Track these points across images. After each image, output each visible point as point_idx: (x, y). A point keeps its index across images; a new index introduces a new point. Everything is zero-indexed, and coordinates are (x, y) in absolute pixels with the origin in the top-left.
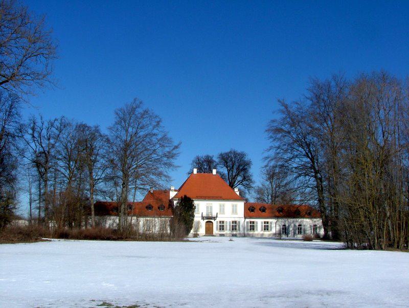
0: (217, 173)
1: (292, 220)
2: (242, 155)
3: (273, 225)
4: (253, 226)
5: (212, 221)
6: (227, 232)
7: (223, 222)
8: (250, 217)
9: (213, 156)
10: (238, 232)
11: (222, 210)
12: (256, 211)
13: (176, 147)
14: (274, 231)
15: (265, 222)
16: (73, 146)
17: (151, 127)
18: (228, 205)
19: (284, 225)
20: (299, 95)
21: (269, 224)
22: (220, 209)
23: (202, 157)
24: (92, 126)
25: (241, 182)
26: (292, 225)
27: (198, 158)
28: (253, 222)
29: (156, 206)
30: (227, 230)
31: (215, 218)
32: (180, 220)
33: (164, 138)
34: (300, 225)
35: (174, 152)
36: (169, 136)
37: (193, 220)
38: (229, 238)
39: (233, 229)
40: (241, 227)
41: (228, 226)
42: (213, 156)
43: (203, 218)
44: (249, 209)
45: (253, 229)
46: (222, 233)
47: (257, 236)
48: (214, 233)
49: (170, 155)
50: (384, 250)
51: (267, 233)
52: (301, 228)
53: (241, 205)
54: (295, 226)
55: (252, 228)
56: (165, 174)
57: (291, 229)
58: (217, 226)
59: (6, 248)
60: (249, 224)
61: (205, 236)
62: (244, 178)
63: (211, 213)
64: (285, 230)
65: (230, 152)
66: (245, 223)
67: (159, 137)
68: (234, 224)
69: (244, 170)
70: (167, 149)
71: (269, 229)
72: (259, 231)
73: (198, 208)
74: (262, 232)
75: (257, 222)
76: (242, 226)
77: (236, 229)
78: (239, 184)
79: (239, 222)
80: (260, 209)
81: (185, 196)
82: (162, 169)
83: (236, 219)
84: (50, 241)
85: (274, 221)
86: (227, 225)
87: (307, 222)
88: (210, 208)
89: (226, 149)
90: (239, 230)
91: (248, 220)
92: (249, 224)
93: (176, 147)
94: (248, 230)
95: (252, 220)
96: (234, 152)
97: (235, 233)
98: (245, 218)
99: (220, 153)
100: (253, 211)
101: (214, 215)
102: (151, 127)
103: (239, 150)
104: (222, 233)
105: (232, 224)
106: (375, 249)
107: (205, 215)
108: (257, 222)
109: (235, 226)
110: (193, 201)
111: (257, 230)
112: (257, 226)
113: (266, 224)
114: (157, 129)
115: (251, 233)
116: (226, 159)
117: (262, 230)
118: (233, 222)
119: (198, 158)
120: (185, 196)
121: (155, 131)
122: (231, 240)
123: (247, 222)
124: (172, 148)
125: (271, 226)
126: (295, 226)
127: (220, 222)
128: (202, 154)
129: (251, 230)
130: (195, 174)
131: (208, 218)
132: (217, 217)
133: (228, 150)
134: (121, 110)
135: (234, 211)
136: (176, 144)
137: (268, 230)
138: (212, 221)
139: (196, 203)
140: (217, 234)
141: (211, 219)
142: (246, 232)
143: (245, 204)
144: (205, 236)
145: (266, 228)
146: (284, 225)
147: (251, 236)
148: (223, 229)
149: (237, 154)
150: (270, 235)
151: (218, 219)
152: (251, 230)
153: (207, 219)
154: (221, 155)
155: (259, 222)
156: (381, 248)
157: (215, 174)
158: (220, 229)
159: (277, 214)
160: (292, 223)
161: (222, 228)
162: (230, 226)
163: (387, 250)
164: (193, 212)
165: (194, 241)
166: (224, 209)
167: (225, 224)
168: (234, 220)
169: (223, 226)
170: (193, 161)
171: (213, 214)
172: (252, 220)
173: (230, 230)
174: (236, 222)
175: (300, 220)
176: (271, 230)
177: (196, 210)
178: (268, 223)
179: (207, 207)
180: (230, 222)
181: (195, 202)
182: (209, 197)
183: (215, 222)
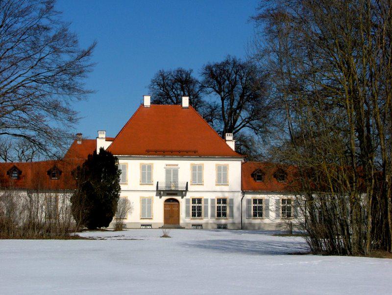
4: (260, 208)
5: (178, 198)
6: (208, 219)
7: (200, 201)
8: (255, 191)
9: (191, 71)
10: (230, 220)
11: (197, 177)
12: (266, 178)
13: (86, 53)
17: (35, 14)
18: (210, 167)
22: (194, 176)
25: (248, 122)
27: (162, 75)
28: (261, 201)
30: (206, 215)
32: (95, 199)
33: (62, 35)
35: (83, 62)
36: (71, 30)
37: (117, 196)
38: (161, 232)
39: (219, 215)
40: (235, 210)
41: (209, 210)
42: (191, 71)
43: (159, 193)
44: (253, 175)
45: (261, 215)
46: (197, 221)
47: (266, 229)
48: (181, 222)
49: (72, 70)
50: (367, 256)
53: (235, 168)
55: (259, 211)
56: (64, 105)
58: (187, 207)
60: (253, 205)
61: (162, 228)
63: (176, 182)
65: (227, 63)
66: (244, 203)
67: (51, 34)
68: (221, 205)
70: (66, 58)
71: (203, 214)
72: (272, 218)
73: (125, 175)
75: (268, 201)
76: (238, 208)
77: (225, 215)
78: (244, 126)
79: (232, 200)
82: (63, 99)
83: (228, 196)
86: (206, 207)
88: (172, 174)
90: (232, 216)
91: (249, 197)
92: (253, 205)
93: (86, 53)
94: (249, 216)
95: (258, 196)
96: (235, 62)
97: (223, 221)
98: (244, 191)
99: (206, 64)
100: (260, 178)
101: (181, 186)
102: (35, 14)
104: (197, 221)
105: (217, 205)
106: (351, 254)
107: (162, 186)
108: (268, 201)
109: (222, 207)
110: (116, 159)
114: (47, 17)
115: (257, 221)
116: (218, 76)
118: (219, 201)
119: (162, 75)
121: (44, 22)
122: (165, 236)
123: (249, 201)
124: (75, 55)
127: (194, 200)
128: (171, 66)
129: (255, 215)
130: (185, 108)
131: (168, 192)
133: (220, 60)
135: (222, 178)
136: (83, 46)
138: (178, 198)
140: (187, 224)
141: (176, 194)
142: (246, 221)
143: (242, 164)
144: (162, 228)
147: (257, 228)
148: (200, 215)
149: (221, 65)
151: (189, 196)
152: (255, 215)
153: (168, 194)
154: (209, 68)
155: (272, 200)
156: (361, 253)
158: (194, 215)
161: (197, 212)
162: (213, 207)
163: (373, 256)
164: (117, 181)
166: (200, 176)
167: (203, 205)
168: (220, 196)
169: (200, 208)
170: (153, 82)
171: (180, 185)
172: (258, 196)
173: (212, 216)
174: (225, 201)
177: (121, 176)
179: (168, 172)
180: (213, 200)
181: (121, 161)
182: (179, 152)
183: (182, 202)
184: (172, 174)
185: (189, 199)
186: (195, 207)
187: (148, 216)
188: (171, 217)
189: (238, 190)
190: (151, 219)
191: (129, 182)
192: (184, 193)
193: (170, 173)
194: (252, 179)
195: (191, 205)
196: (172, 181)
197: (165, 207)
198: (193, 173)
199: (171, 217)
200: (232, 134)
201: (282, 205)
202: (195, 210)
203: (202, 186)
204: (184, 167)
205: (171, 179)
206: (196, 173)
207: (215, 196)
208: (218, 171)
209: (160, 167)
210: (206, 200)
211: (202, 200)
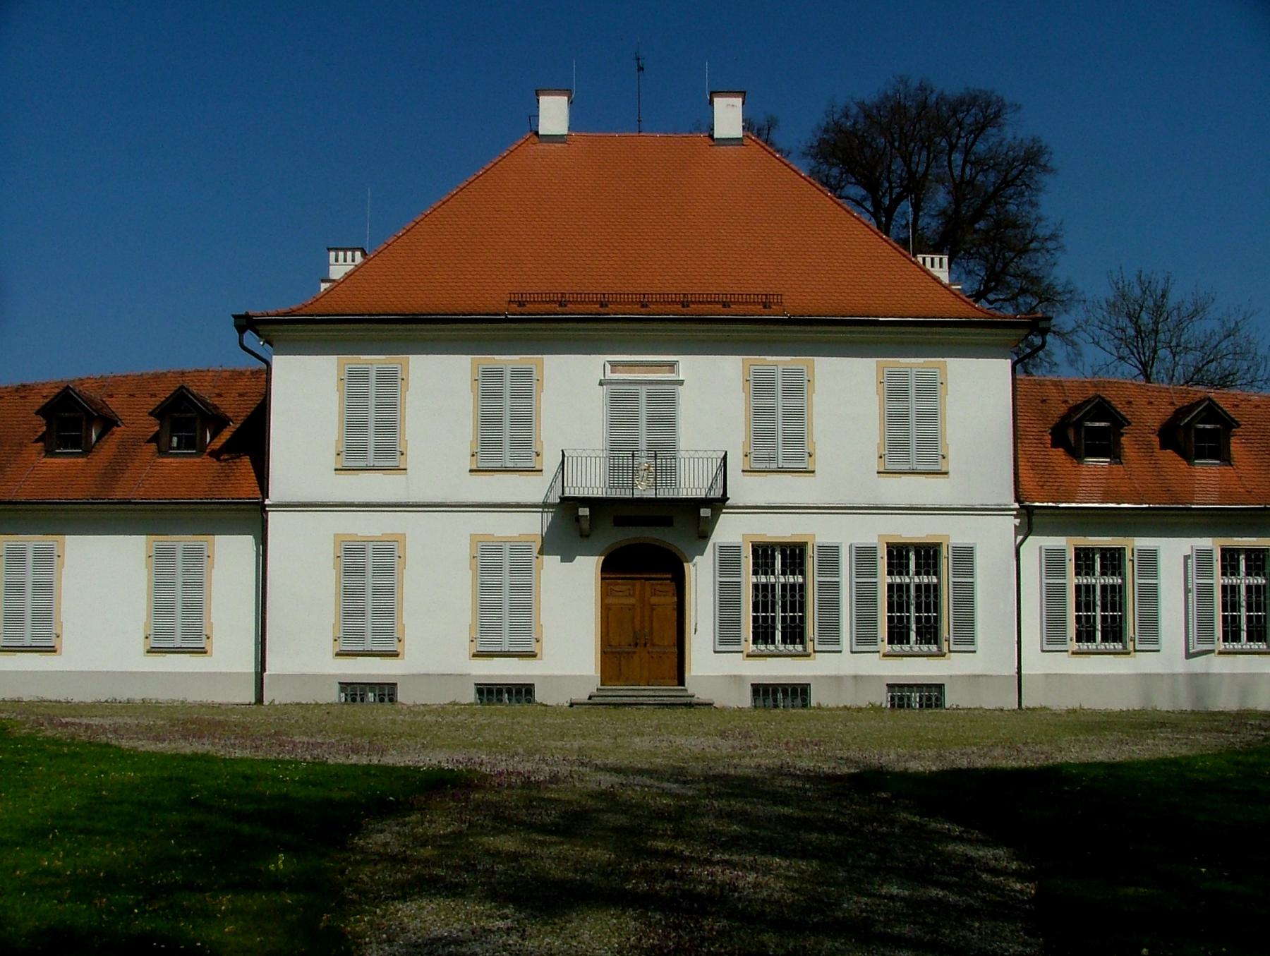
0: (748, 125)
7: (794, 555)
11: (780, 439)
15: (1084, 559)
18: (845, 392)
23: (1034, 205)
31: (695, 516)
44: (1059, 437)
53: (977, 394)
68: (778, 579)
71: (1131, 626)
86: (830, 595)
88: (643, 421)
107: (591, 481)
112: (966, 594)
113: (912, 579)
118: (898, 555)
127: (763, 554)
132: (718, 504)
135: (911, 442)
137: (1114, 632)
141: (666, 522)
151: (730, 530)
157: (736, 131)
167: (813, 578)
180: (864, 555)
184: (643, 421)
185: (873, 550)
186: (1089, 589)
187: (34, 638)
188: (640, 641)
189: (991, 501)
190: (532, 655)
191: (412, 460)
192: (705, 512)
193: (635, 410)
194: (1059, 454)
195: (884, 579)
196: (643, 444)
197: (606, 593)
198: (484, 408)
199: (640, 641)
200: (945, 259)
201: (888, 580)
202: (1089, 606)
203: (939, 480)
204: (711, 396)
205: (636, 442)
206: (773, 410)
207: (877, 532)
208: (485, 395)
209: (574, 398)
210: (830, 554)
211: (809, 551)
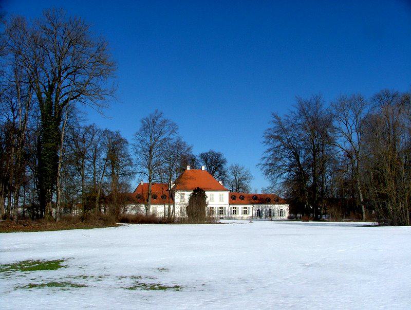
1: (264, 205)
2: (219, 155)
3: (251, 210)
8: (233, 204)
14: (251, 215)
16: (355, 137)
19: (259, 210)
20: (287, 110)
21: (247, 209)
24: (114, 131)
26: (264, 209)
28: (235, 208)
29: (159, 196)
34: (270, 210)
44: (231, 198)
45: (236, 213)
51: (245, 216)
52: (246, 211)
53: (226, 195)
54: (266, 210)
55: (235, 212)
57: (264, 213)
59: (69, 233)
62: (220, 174)
64: (259, 214)
69: (220, 166)
72: (240, 214)
74: (242, 216)
77: (222, 214)
80: (240, 198)
81: (198, 188)
84: (123, 225)
85: (251, 206)
87: (276, 207)
89: (206, 150)
91: (231, 206)
95: (234, 206)
97: (222, 216)
100: (234, 199)
103: (216, 151)
111: (238, 214)
112: (238, 211)
115: (233, 216)
117: (242, 214)
120: (198, 188)
121: (171, 137)
123: (231, 208)
125: (249, 211)
126: (266, 210)
134: (147, 119)
135: (221, 199)
139: (207, 193)
145: (245, 212)
146: (259, 210)
150: (248, 217)
154: (202, 154)
155: (240, 208)
159: (253, 201)
160: (264, 208)
165: (346, 226)
168: (221, 206)
172: (234, 206)
174: (222, 208)
175: (269, 206)
176: (249, 213)
178: (246, 208)
